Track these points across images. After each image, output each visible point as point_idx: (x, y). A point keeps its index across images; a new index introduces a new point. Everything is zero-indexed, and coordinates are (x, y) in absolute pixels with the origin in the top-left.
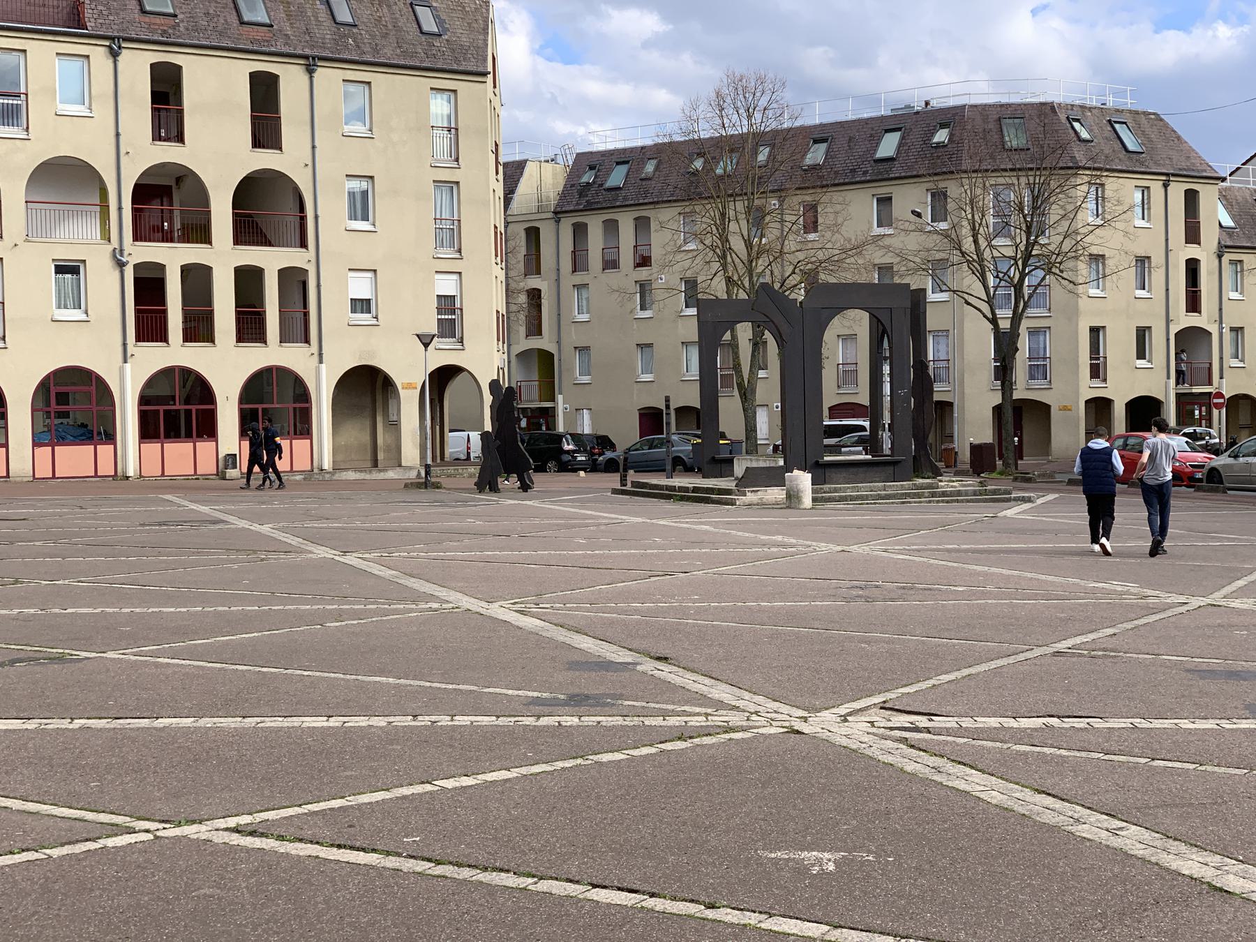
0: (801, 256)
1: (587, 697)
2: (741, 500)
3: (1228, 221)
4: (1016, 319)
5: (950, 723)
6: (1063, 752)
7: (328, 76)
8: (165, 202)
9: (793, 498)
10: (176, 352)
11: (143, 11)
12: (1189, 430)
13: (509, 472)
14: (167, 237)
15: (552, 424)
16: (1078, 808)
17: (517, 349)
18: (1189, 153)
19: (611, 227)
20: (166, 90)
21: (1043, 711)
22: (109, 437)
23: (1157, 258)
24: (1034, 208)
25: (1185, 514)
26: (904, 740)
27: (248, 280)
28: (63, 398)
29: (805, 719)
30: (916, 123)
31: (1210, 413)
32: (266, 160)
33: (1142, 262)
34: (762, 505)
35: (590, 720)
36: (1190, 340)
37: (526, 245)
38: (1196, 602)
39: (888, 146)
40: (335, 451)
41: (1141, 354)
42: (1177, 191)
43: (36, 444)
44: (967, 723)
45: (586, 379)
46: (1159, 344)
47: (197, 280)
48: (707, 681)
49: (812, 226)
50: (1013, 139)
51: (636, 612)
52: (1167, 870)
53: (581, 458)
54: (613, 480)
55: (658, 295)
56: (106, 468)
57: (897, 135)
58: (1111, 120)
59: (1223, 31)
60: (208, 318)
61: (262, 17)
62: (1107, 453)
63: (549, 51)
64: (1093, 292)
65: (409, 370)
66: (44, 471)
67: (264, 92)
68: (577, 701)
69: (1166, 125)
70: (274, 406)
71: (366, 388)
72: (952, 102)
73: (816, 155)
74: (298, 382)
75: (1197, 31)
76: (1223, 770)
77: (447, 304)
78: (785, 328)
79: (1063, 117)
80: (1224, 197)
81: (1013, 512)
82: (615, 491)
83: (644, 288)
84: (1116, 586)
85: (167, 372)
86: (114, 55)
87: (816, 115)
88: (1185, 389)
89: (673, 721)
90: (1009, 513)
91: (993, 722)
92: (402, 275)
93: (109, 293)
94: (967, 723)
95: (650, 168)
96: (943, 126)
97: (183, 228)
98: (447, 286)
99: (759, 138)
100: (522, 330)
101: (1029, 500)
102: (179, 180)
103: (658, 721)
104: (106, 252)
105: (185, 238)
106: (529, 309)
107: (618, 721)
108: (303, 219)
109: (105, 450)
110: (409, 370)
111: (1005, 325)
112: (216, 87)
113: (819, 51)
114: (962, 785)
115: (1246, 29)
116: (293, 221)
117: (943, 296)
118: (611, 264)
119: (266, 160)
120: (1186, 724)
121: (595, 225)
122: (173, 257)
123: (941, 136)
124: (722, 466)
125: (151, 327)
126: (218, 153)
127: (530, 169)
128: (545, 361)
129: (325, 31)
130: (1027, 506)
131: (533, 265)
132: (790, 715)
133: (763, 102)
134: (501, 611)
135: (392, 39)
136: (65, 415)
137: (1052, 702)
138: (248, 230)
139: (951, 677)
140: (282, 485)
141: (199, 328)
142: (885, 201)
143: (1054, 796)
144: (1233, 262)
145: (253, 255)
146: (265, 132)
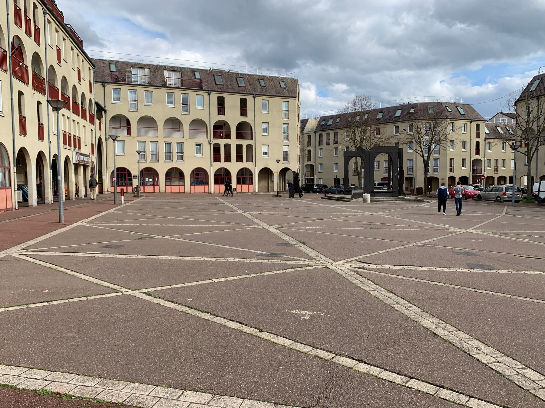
0: (374, 140)
1: (275, 254)
2: (352, 201)
3: (487, 132)
4: (429, 156)
5: (374, 266)
6: (404, 278)
7: (259, 99)
8: (221, 129)
9: (365, 200)
10: (222, 164)
11: (216, 84)
12: (475, 185)
13: (296, 193)
14: (222, 138)
15: (313, 182)
16: (400, 298)
17: (305, 164)
18: (478, 114)
19: (328, 135)
20: (221, 103)
21: (404, 264)
22: (207, 184)
23: (468, 141)
24: (434, 128)
25: (466, 206)
26: (357, 272)
27: (239, 148)
28: (198, 175)
29: (332, 264)
30: (406, 108)
31: (481, 180)
32: (244, 119)
33: (464, 142)
34: (357, 202)
35: (271, 261)
36: (476, 162)
37: (307, 139)
38: (465, 231)
39: (398, 113)
40: (258, 188)
41: (463, 166)
42: (474, 124)
43: (191, 185)
44: (379, 267)
45: (321, 171)
46: (468, 163)
47: (227, 147)
48: (311, 250)
49: (378, 133)
50: (430, 111)
51: (306, 229)
52: (419, 325)
53: (318, 190)
54: (323, 195)
55: (339, 150)
56: (207, 191)
57: (401, 111)
58: (456, 106)
59: (490, 86)
60: (230, 156)
61: (243, 85)
62: (445, 190)
63: (320, 94)
64: (451, 150)
65: (276, 169)
66: (193, 191)
67: (244, 102)
68: (273, 255)
69: (472, 108)
70: (245, 177)
71: (266, 173)
72: (415, 102)
73: (380, 116)
74: (251, 171)
75: (483, 86)
76: (452, 286)
77: (286, 153)
78: (364, 158)
79: (444, 106)
80: (487, 126)
81: (423, 205)
82: (322, 198)
83: (336, 149)
84: (443, 226)
85: (221, 169)
86: (209, 94)
87: (379, 106)
88: (475, 175)
89: (294, 262)
90: (422, 205)
91: (387, 267)
92: (275, 147)
93: (208, 151)
94: (379, 267)
95: (338, 120)
96: (413, 108)
97: (225, 135)
98: (286, 149)
99: (364, 113)
100: (306, 160)
101: (429, 202)
102: (225, 124)
103: (290, 262)
104: (206, 140)
105: (226, 138)
106: (307, 155)
107: (279, 262)
108: (252, 133)
109: (206, 187)
110: (276, 169)
111: (426, 158)
112: (232, 102)
113: (386, 92)
114: (366, 288)
115: (496, 85)
116: (250, 133)
117: (412, 151)
118: (328, 144)
119: (244, 119)
120: (446, 270)
121: (324, 134)
122: (222, 142)
123: (412, 111)
124: (348, 192)
125: (217, 158)
126: (233, 117)
127: (309, 121)
128: (312, 166)
129: (258, 88)
130: (428, 203)
131: (309, 144)
132: (327, 262)
133: (365, 103)
134: (272, 229)
135: (274, 89)
136: (198, 178)
137: (408, 261)
138: (239, 136)
139: (382, 252)
140: (232, 196)
141: (228, 159)
142: (397, 127)
143: (394, 294)
144: (489, 142)
145: (240, 142)
146: (244, 112)
